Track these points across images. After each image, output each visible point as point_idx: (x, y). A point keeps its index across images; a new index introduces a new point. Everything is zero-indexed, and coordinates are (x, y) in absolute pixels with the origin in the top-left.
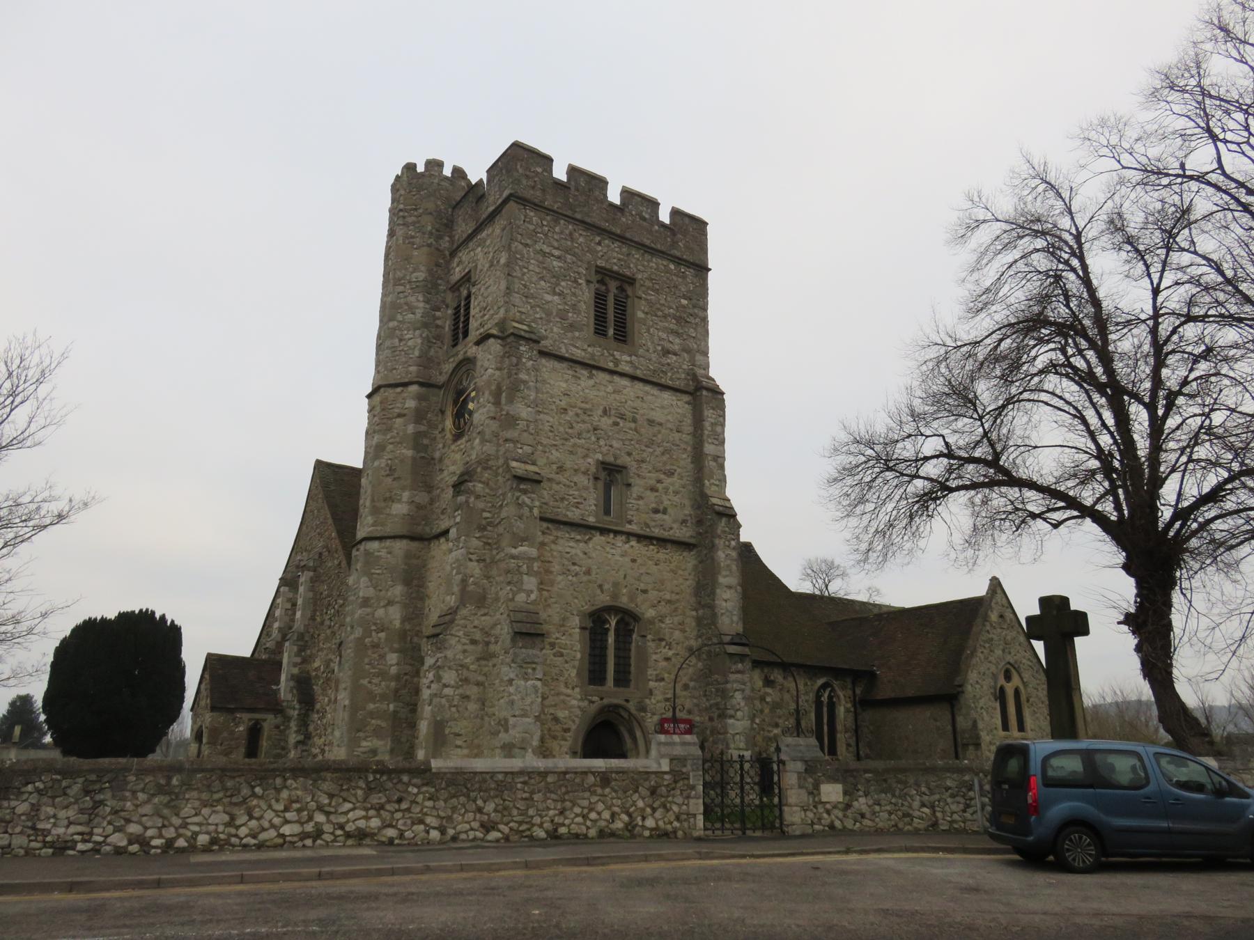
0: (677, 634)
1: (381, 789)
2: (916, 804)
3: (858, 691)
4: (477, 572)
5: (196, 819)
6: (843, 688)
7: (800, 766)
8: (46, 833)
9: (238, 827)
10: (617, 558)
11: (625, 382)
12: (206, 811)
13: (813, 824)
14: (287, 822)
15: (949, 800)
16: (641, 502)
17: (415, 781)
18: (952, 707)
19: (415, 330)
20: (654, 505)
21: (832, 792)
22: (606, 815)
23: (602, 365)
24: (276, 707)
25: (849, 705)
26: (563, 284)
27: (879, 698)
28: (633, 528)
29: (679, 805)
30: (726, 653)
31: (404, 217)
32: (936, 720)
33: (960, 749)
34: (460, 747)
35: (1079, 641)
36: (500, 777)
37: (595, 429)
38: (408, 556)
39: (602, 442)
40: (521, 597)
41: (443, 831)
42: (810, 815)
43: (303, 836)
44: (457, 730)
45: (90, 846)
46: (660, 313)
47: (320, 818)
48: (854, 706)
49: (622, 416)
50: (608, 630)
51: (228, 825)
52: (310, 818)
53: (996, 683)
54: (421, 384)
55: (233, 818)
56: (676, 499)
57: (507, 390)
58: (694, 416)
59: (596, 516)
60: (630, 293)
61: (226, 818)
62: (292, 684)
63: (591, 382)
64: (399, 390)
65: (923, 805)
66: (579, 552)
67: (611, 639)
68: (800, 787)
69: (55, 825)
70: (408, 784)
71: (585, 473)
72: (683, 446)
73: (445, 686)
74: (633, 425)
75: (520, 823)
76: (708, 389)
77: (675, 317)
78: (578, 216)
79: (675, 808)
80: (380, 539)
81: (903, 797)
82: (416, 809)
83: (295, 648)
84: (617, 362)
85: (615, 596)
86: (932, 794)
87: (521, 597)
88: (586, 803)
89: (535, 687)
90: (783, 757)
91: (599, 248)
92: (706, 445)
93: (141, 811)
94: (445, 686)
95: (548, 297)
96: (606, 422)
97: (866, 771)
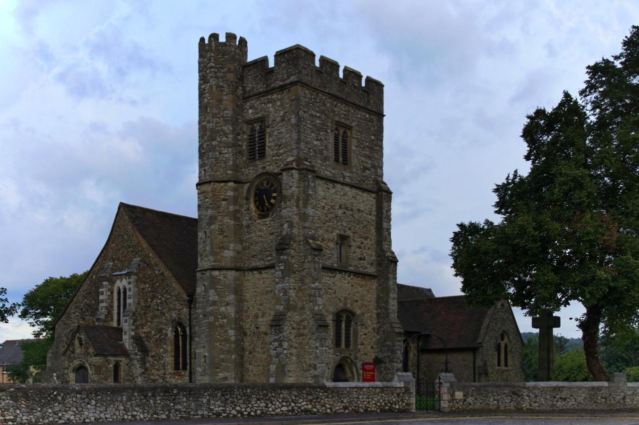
0: (369, 322)
1: (311, 394)
2: (491, 400)
3: (420, 344)
4: (293, 295)
5: (257, 405)
6: (413, 343)
7: (448, 385)
8: (212, 410)
9: (268, 408)
10: (346, 284)
11: (347, 189)
12: (259, 402)
13: (452, 407)
14: (283, 406)
15: (505, 398)
16: (354, 255)
17: (321, 391)
18: (475, 354)
19: (229, 148)
20: (359, 256)
21: (459, 395)
22: (383, 404)
23: (338, 180)
24: (125, 353)
25: (415, 352)
26: (321, 133)
27: (432, 348)
28: (351, 268)
29: (407, 400)
30: (394, 332)
31: (215, 73)
32: (464, 360)
33: (477, 376)
34: (290, 376)
35: (520, 308)
36: (348, 389)
37: (336, 217)
38: (236, 279)
39: (339, 224)
40: (316, 308)
41: (331, 409)
42: (451, 404)
43: (289, 411)
44: (289, 369)
45: (226, 414)
46: (362, 146)
47: (293, 405)
48: (418, 352)
49: (347, 208)
50: (342, 320)
51: (266, 407)
52: (290, 405)
53: (497, 341)
54: (235, 182)
55: (267, 404)
56: (369, 252)
57: (305, 199)
58: (377, 205)
59: (337, 264)
60: (349, 134)
61: (265, 405)
62: (132, 341)
63: (334, 191)
64: (222, 184)
65: (494, 400)
66: (331, 283)
67: (343, 326)
68: (448, 393)
69: (215, 407)
70: (320, 392)
71: (332, 241)
72: (372, 223)
73: (284, 349)
74: (351, 212)
75: (356, 407)
76: (385, 191)
77: (368, 147)
78: (327, 90)
79: (406, 401)
80: (220, 269)
81: (486, 397)
82: (322, 401)
83: (132, 321)
84: (344, 177)
85: (345, 304)
86: (498, 395)
87: (316, 308)
88: (376, 399)
89: (326, 350)
90: (441, 381)
91: (336, 109)
92: (384, 223)
93: (239, 402)
94: (284, 349)
95: (315, 143)
96: (340, 212)
97: (473, 387)
